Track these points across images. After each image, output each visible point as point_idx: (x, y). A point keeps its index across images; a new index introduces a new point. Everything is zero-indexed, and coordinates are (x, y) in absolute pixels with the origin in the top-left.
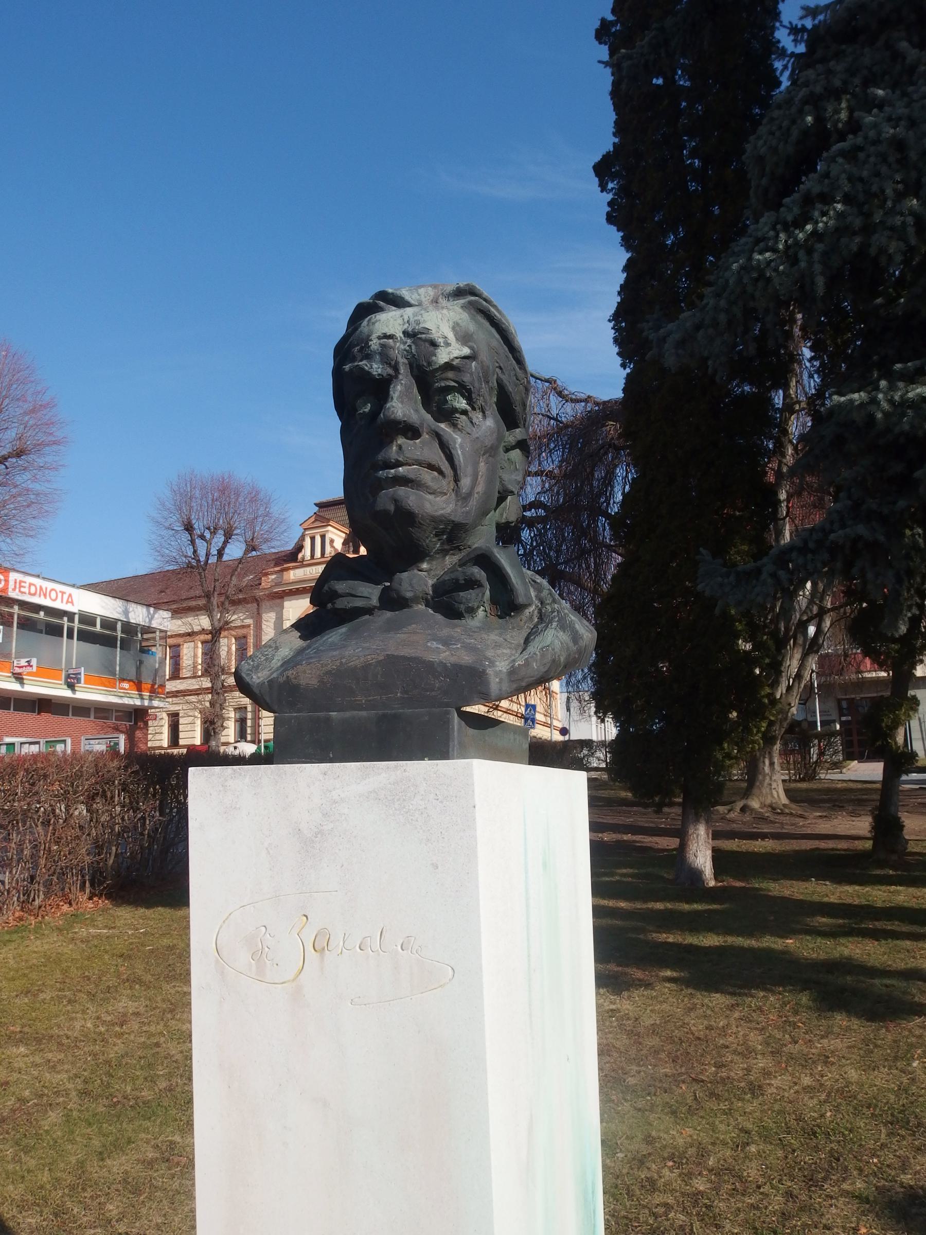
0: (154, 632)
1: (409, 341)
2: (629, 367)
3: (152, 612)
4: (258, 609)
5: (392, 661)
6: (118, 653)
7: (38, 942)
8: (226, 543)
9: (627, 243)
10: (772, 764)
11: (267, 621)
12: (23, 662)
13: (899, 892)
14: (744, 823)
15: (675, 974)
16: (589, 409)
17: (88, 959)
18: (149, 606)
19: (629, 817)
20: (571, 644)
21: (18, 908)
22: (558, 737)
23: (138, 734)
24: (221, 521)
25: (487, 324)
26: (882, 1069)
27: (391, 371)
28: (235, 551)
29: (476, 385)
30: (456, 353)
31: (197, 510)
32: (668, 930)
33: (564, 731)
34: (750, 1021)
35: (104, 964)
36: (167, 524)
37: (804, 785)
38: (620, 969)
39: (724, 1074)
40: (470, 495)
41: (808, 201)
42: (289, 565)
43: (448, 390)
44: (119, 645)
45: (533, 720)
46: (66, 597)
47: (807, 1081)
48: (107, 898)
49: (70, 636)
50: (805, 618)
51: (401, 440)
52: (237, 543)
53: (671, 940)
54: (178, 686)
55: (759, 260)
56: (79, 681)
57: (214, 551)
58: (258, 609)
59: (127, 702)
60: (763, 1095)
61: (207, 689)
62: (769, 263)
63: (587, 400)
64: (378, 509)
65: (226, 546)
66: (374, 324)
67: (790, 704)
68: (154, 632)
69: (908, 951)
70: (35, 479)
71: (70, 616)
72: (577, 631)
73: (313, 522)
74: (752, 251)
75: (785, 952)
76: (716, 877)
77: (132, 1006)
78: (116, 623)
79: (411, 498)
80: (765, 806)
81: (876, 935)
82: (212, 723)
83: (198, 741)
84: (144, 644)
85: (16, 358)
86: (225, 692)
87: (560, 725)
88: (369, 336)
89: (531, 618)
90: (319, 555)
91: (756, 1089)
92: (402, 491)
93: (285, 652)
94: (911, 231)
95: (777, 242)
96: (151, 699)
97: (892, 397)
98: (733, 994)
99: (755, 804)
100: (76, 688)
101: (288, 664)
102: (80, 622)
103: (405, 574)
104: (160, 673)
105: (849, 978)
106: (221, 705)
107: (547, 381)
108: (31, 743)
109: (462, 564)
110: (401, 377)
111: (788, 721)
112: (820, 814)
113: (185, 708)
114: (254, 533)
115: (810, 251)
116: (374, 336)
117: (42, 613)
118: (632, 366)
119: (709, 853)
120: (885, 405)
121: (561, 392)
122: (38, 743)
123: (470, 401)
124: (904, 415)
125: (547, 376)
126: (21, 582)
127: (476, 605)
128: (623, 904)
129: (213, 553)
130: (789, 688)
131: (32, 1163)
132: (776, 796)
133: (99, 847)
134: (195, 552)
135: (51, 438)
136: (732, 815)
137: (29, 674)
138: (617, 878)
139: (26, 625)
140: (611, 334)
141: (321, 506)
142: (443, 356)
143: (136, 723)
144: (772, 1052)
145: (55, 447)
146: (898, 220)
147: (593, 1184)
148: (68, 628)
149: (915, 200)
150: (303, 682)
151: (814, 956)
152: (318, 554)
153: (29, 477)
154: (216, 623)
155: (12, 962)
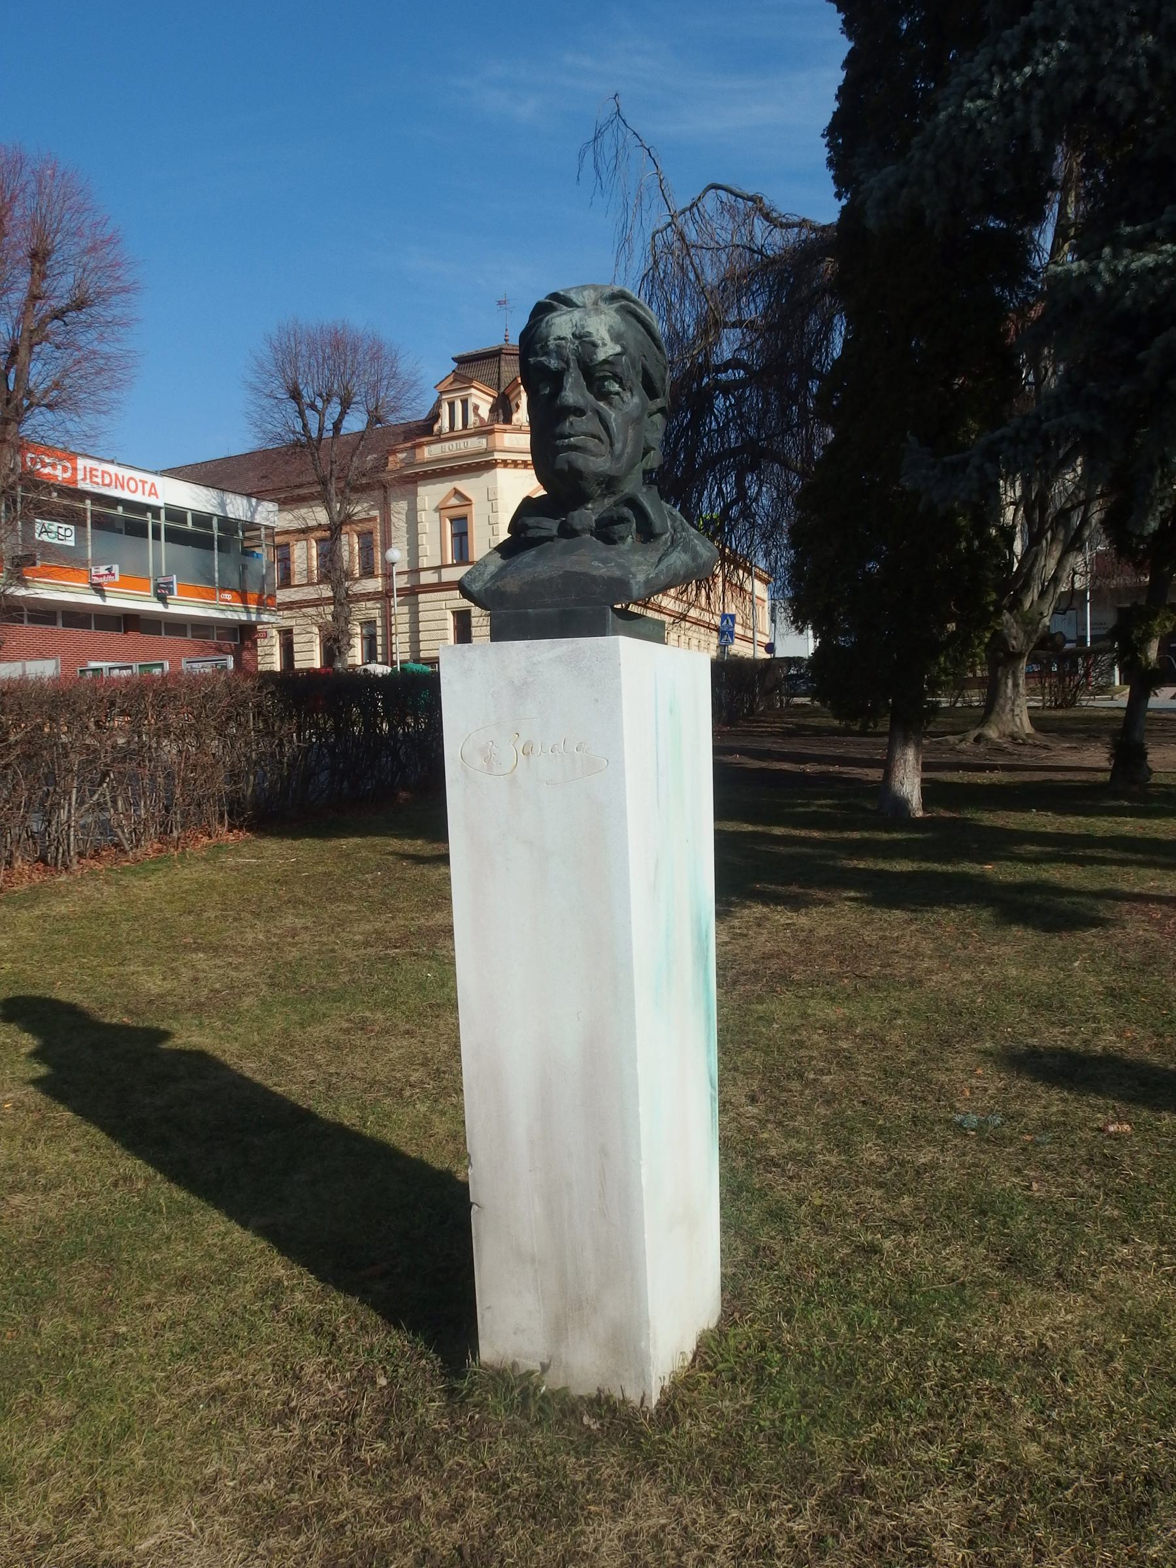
0: (259, 529)
1: (577, 342)
2: (845, 197)
3: (254, 504)
4: (385, 498)
5: (569, 576)
6: (216, 556)
7: (186, 871)
8: (343, 414)
9: (849, 27)
10: (1016, 685)
11: (399, 513)
12: (103, 570)
13: (1126, 823)
14: (976, 755)
15: (858, 895)
16: (803, 237)
17: (244, 884)
18: (249, 495)
19: (840, 748)
20: (690, 562)
21: (156, 840)
22: (762, 654)
23: (246, 655)
24: (336, 386)
25: (634, 321)
26: (1042, 968)
27: (564, 365)
28: (355, 423)
29: (626, 373)
30: (611, 352)
31: (305, 372)
32: (861, 857)
33: (770, 648)
34: (926, 933)
35: (261, 888)
36: (267, 391)
37: (1060, 713)
38: (802, 890)
39: (888, 971)
40: (621, 455)
41: (1030, 36)
42: (422, 440)
43: (606, 378)
44: (216, 546)
45: (732, 634)
46: (147, 487)
47: (967, 977)
48: (247, 831)
49: (156, 536)
50: (1069, 505)
51: (572, 418)
52: (357, 414)
53: (861, 866)
54: (293, 597)
55: (969, 109)
56: (171, 592)
57: (329, 425)
58: (385, 498)
59: (230, 617)
60: (921, 987)
61: (329, 598)
62: (980, 112)
63: (802, 224)
64: (556, 468)
65: (343, 418)
66: (551, 326)
67: (1041, 614)
68: (259, 529)
69: (1111, 875)
70: (101, 339)
71: (156, 511)
72: (697, 552)
73: (451, 384)
74: (963, 97)
75: (982, 876)
76: (925, 805)
77: (299, 923)
78: (211, 519)
79: (580, 461)
80: (1004, 735)
81: (1081, 862)
82: (336, 640)
83: (317, 664)
84: (246, 544)
85: (66, 178)
86: (351, 602)
87: (766, 640)
88: (548, 337)
89: (666, 543)
90: (460, 427)
91: (915, 983)
92: (573, 455)
93: (492, 569)
94: (1144, 73)
95: (991, 87)
96: (259, 613)
97: (1115, 267)
98: (913, 911)
99: (992, 733)
100: (168, 601)
101: (495, 577)
102: (167, 518)
103: (576, 513)
104: (269, 580)
105: (1038, 897)
106: (346, 618)
107: (750, 199)
108: (121, 668)
109: (616, 504)
110: (571, 370)
111: (1038, 635)
112: (1068, 745)
113: (300, 621)
114: (377, 400)
115: (1027, 98)
116: (552, 337)
117: (120, 509)
118: (849, 196)
119: (917, 780)
120: (1107, 277)
121: (768, 214)
122: (130, 667)
123: (621, 385)
124: (1127, 288)
125: (750, 191)
126: (92, 470)
127: (626, 534)
128: (816, 834)
129: (328, 428)
130: (1042, 594)
131: (241, 1030)
132: (1018, 723)
133: (234, 776)
134: (305, 426)
135: (117, 284)
136: (963, 746)
137: (110, 584)
138: (814, 808)
139: (103, 523)
140: (825, 153)
141: (461, 361)
142: (602, 355)
143: (242, 642)
144: (940, 956)
145: (124, 296)
146: (1129, 62)
147: (707, 931)
148: (153, 526)
149: (1151, 37)
150: (508, 589)
151: (1010, 879)
152: (459, 424)
153: (96, 336)
154: (336, 517)
155: (164, 888)
